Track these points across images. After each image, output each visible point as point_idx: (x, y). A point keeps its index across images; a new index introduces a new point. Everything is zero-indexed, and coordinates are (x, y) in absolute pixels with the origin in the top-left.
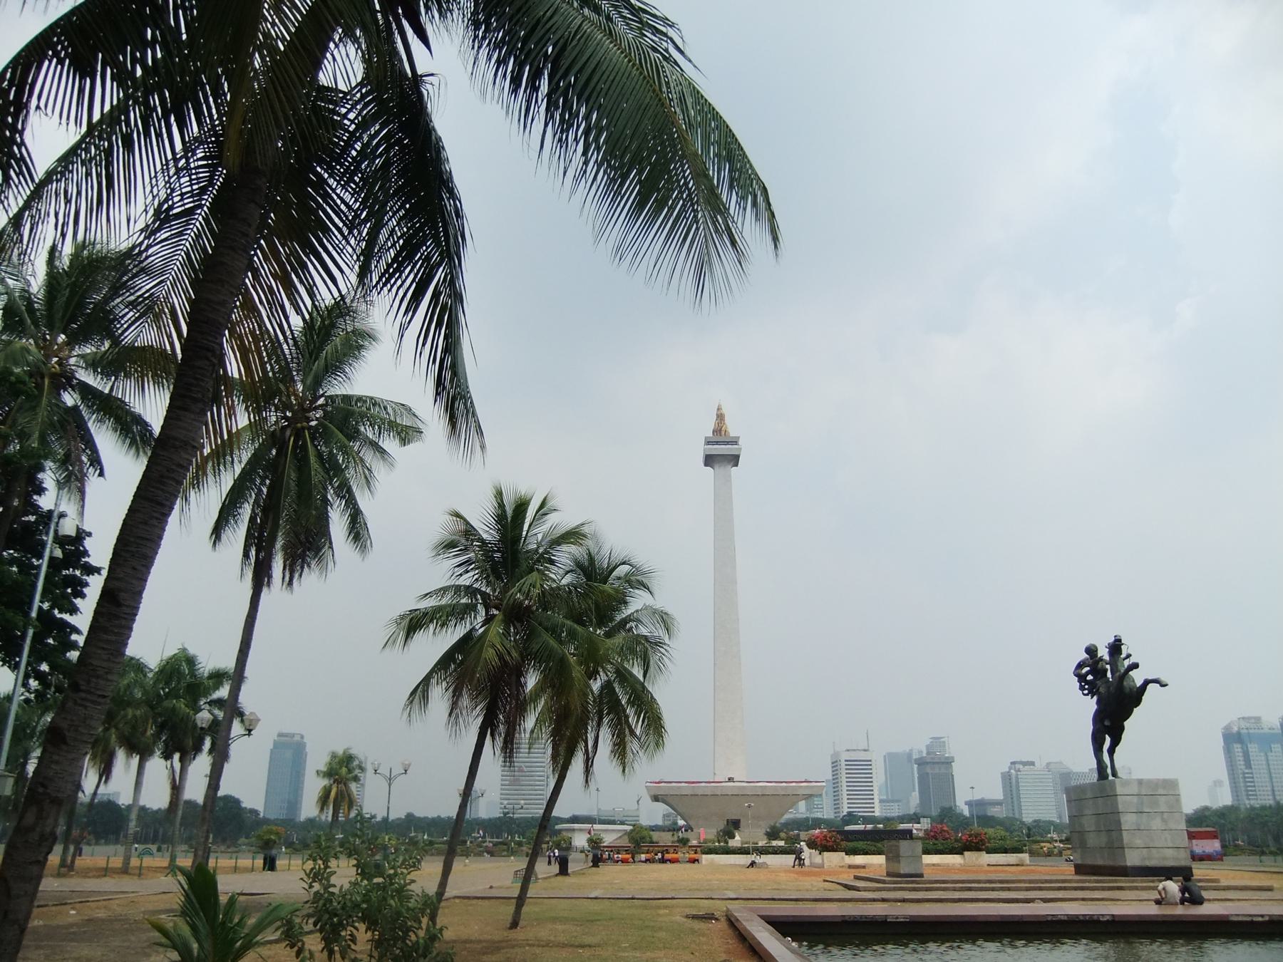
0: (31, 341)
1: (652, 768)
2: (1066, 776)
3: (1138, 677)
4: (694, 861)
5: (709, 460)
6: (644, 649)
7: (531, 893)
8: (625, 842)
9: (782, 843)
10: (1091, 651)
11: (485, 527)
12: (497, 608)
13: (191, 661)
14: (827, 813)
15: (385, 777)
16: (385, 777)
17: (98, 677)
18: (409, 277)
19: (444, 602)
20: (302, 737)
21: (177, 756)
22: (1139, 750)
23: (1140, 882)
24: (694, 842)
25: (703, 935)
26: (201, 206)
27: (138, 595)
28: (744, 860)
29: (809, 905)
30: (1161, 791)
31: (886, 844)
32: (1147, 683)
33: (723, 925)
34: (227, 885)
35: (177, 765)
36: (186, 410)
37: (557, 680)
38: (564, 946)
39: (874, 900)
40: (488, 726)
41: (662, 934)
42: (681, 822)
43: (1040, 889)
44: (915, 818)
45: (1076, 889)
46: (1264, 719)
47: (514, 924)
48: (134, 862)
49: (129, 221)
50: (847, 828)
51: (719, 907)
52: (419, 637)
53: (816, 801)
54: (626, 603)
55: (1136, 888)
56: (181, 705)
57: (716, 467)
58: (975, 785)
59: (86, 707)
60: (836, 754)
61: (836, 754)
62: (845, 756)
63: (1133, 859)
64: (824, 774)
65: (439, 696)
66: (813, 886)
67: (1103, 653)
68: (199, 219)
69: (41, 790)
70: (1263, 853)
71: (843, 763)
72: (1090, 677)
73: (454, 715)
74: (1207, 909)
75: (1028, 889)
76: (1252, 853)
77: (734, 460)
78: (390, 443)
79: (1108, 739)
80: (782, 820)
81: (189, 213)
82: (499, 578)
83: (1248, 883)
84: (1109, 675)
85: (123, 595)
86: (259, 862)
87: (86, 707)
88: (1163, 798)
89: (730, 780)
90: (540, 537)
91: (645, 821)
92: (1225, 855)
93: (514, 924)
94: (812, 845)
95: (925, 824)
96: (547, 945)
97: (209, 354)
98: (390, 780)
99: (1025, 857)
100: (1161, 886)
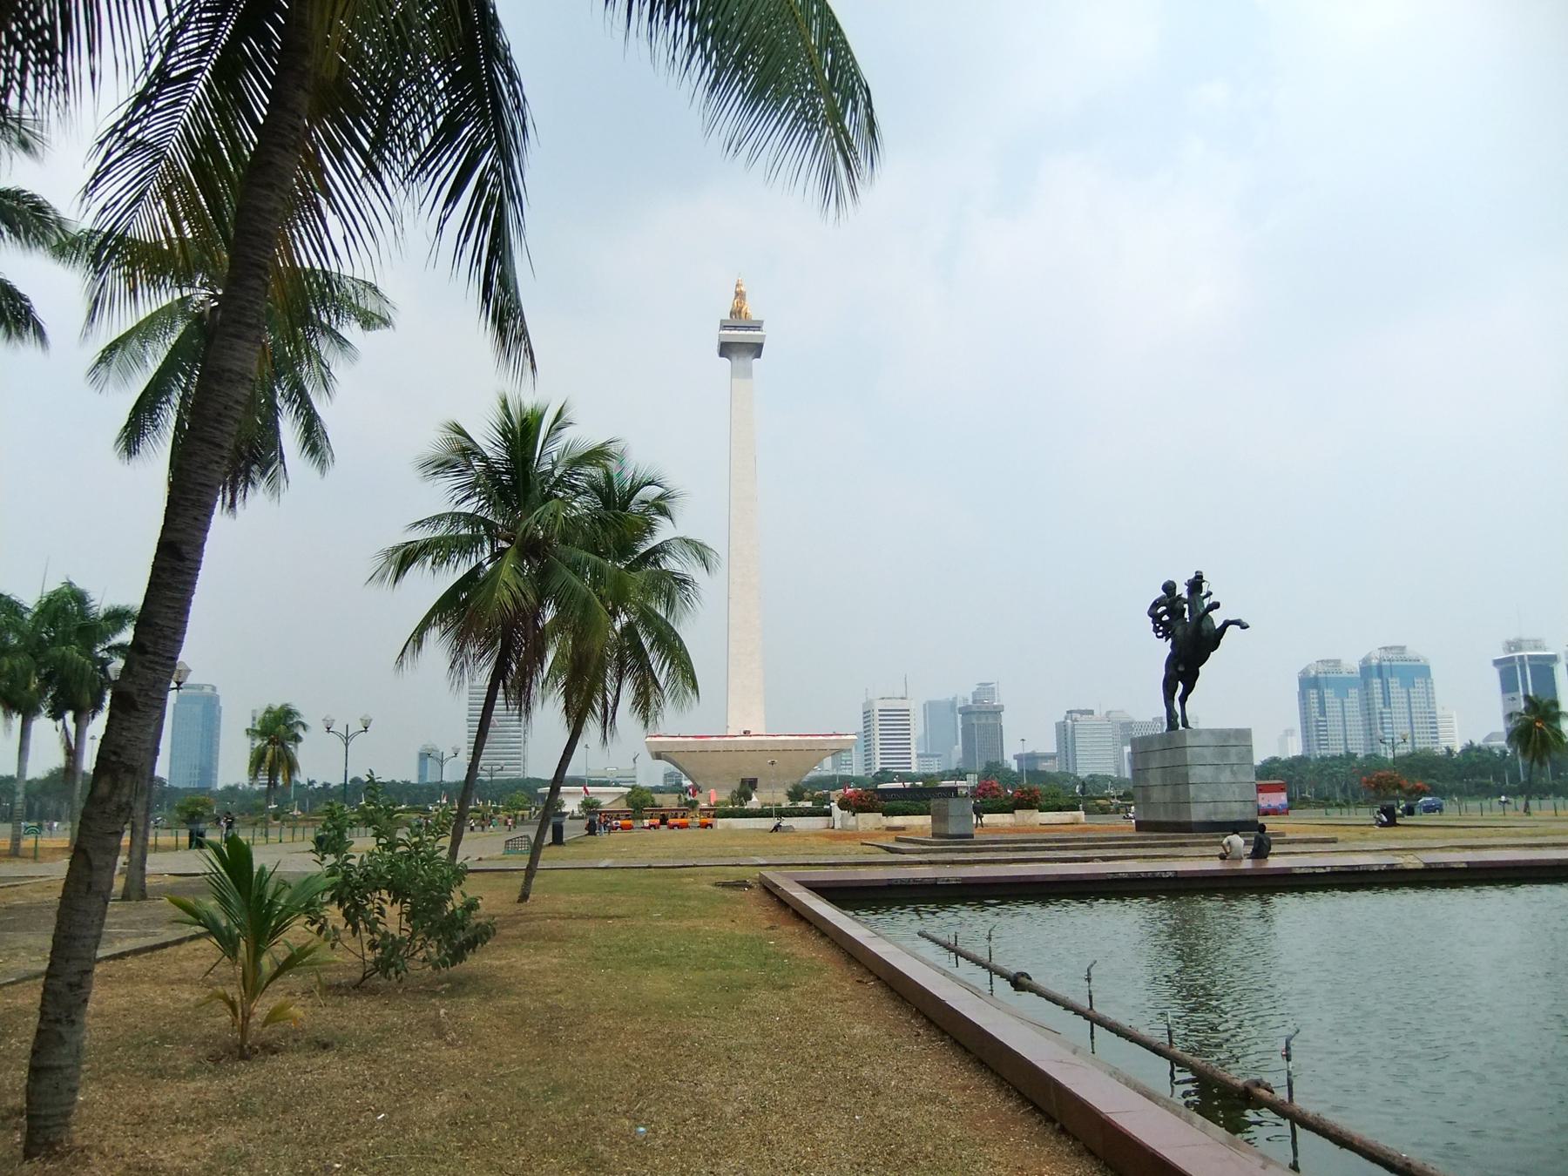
1: (679, 722)
2: (1127, 726)
3: (1218, 618)
4: (705, 826)
5: (726, 349)
6: (672, 587)
7: (541, 864)
8: (622, 806)
9: (809, 804)
10: (1169, 588)
11: (486, 437)
12: (507, 540)
13: (80, 598)
14: (857, 770)
15: (340, 735)
16: (340, 735)
17: (165, 637)
18: (450, 165)
19: (438, 534)
20: (214, 689)
21: (69, 715)
22: (1215, 700)
23: (1204, 838)
24: (704, 805)
25: (739, 903)
26: (200, 70)
27: (199, 549)
28: (769, 823)
29: (850, 870)
30: (1233, 742)
31: (933, 803)
32: (1227, 624)
33: (756, 892)
34: (262, 858)
35: (72, 727)
36: (239, 337)
37: (579, 622)
38: (581, 917)
39: (920, 863)
40: (498, 675)
41: (692, 903)
42: (687, 783)
43: (1099, 847)
44: (960, 775)
45: (1137, 846)
46: (1344, 662)
47: (524, 897)
48: (28, 842)
49: (93, 74)
50: (880, 786)
51: (751, 875)
52: (414, 570)
53: (844, 756)
54: (652, 532)
55: (1200, 844)
56: (73, 651)
57: (734, 358)
58: (1026, 737)
59: (155, 670)
60: (869, 703)
61: (869, 703)
62: (878, 705)
63: (1198, 814)
64: (851, 728)
65: (437, 646)
66: (850, 851)
67: (1182, 590)
68: (199, 86)
69: (113, 758)
70: (1331, 806)
71: (877, 713)
72: (1166, 618)
73: (457, 667)
74: (1274, 862)
75: (1086, 848)
76: (1318, 806)
77: (756, 349)
78: (350, 330)
79: (1180, 685)
80: (805, 780)
81: (188, 76)
82: (508, 503)
83: (1313, 836)
84: (1187, 615)
85: (185, 549)
86: (184, 838)
87: (155, 670)
88: (1233, 750)
89: (746, 733)
90: (555, 455)
91: (643, 782)
92: (1290, 808)
93: (524, 897)
94: (843, 805)
95: (972, 780)
96: (570, 917)
97: (262, 272)
98: (347, 740)
99: (1081, 815)
100: (1225, 841)
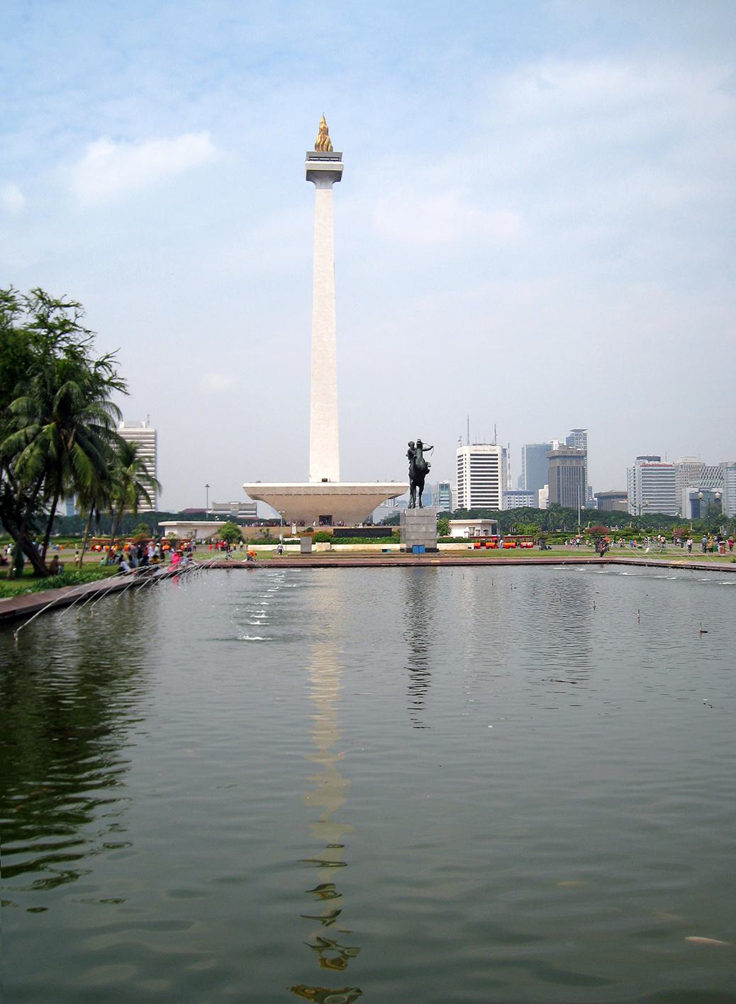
0: (129, 489)
5: (312, 175)
89: (325, 480)
